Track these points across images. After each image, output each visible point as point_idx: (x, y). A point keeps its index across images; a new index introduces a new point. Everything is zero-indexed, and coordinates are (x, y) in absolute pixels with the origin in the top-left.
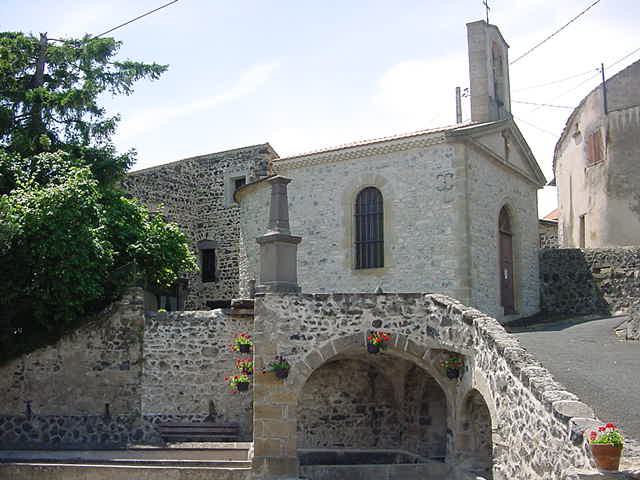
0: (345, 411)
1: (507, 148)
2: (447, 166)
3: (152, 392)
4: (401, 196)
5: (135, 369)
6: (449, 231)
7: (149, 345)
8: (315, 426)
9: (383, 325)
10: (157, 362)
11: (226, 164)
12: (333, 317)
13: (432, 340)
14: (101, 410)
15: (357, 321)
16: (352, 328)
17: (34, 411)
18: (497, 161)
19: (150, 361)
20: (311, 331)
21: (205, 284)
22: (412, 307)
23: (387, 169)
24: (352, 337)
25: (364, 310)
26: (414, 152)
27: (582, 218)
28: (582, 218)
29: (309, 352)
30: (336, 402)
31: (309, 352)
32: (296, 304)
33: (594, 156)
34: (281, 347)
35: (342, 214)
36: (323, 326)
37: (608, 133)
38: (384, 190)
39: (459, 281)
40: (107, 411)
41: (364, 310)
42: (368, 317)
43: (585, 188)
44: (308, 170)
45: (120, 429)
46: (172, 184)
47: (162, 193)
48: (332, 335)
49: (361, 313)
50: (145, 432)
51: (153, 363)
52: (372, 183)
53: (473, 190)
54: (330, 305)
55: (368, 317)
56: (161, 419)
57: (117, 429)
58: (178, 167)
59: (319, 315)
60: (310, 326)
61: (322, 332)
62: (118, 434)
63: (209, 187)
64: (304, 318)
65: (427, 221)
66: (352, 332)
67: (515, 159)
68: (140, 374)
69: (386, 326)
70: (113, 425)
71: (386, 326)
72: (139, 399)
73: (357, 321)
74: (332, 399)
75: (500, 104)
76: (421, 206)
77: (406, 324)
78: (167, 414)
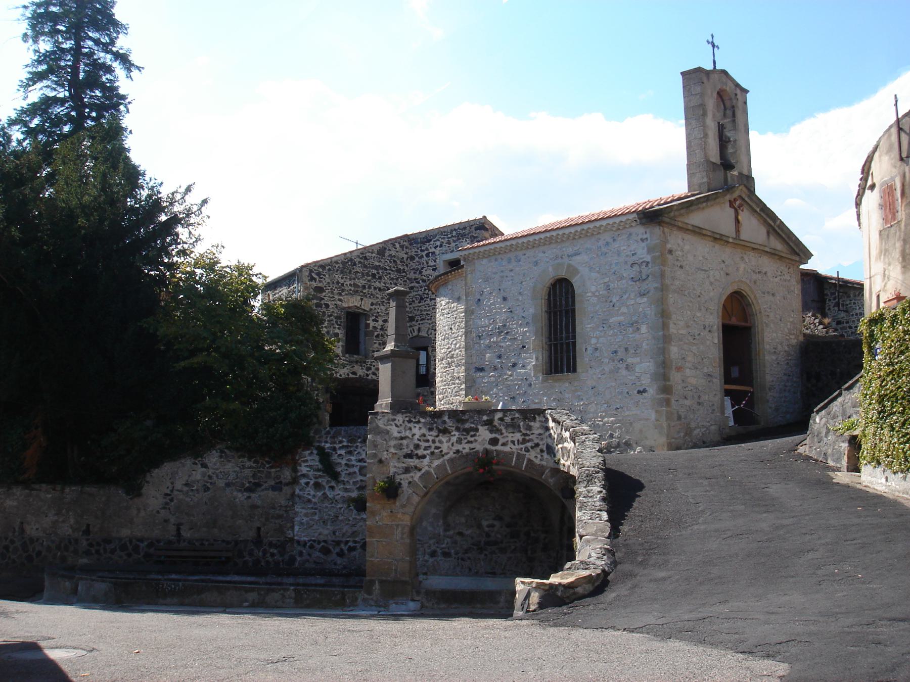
0: (499, 536)
1: (737, 221)
2: (643, 254)
3: (306, 515)
4: (593, 289)
5: (287, 490)
6: (644, 329)
7: (303, 464)
8: (466, 551)
9: (500, 443)
10: (312, 482)
11: (438, 243)
12: (448, 435)
13: (550, 458)
14: (252, 534)
15: (472, 439)
16: (467, 446)
17: (183, 533)
18: (718, 238)
19: (303, 481)
20: (424, 450)
21: (419, 390)
22: (532, 424)
23: (578, 258)
24: (468, 454)
25: (480, 427)
26: (607, 237)
27: (878, 296)
28: (878, 296)
29: (423, 471)
30: (488, 526)
31: (423, 471)
32: (410, 421)
33: (888, 208)
34: (394, 467)
35: (532, 310)
36: (437, 444)
37: (903, 185)
38: (576, 282)
39: (655, 387)
40: (259, 535)
41: (480, 427)
42: (484, 434)
43: (880, 256)
44: (496, 260)
45: (272, 555)
46: (375, 271)
47: (361, 282)
48: (447, 454)
49: (477, 430)
50: (299, 559)
51: (307, 484)
52: (563, 274)
53: (673, 278)
54: (444, 422)
55: (484, 434)
56: (315, 544)
57: (268, 555)
58: (382, 249)
59: (434, 433)
60: (423, 444)
61: (436, 451)
62: (270, 559)
63: (421, 273)
64: (417, 437)
65: (622, 318)
66: (467, 450)
67: (752, 230)
68: (293, 494)
69: (503, 444)
70: (265, 550)
71: (503, 444)
72: (293, 522)
73: (472, 439)
74: (485, 523)
75: (727, 165)
76: (614, 300)
77: (524, 441)
78: (322, 538)
